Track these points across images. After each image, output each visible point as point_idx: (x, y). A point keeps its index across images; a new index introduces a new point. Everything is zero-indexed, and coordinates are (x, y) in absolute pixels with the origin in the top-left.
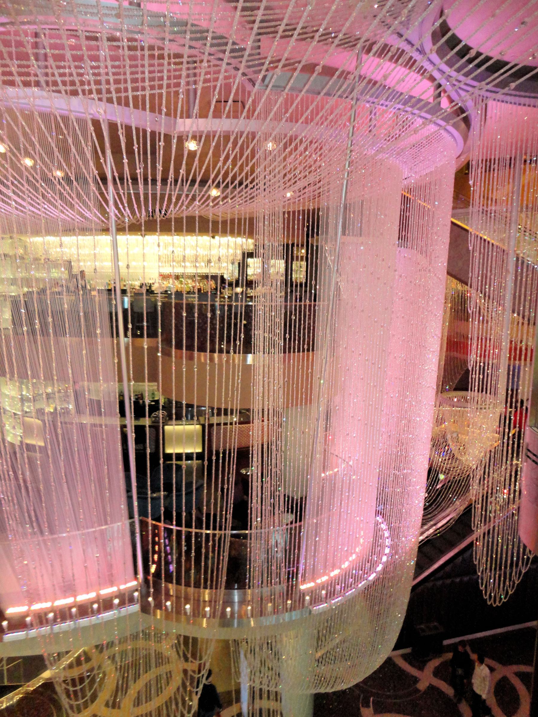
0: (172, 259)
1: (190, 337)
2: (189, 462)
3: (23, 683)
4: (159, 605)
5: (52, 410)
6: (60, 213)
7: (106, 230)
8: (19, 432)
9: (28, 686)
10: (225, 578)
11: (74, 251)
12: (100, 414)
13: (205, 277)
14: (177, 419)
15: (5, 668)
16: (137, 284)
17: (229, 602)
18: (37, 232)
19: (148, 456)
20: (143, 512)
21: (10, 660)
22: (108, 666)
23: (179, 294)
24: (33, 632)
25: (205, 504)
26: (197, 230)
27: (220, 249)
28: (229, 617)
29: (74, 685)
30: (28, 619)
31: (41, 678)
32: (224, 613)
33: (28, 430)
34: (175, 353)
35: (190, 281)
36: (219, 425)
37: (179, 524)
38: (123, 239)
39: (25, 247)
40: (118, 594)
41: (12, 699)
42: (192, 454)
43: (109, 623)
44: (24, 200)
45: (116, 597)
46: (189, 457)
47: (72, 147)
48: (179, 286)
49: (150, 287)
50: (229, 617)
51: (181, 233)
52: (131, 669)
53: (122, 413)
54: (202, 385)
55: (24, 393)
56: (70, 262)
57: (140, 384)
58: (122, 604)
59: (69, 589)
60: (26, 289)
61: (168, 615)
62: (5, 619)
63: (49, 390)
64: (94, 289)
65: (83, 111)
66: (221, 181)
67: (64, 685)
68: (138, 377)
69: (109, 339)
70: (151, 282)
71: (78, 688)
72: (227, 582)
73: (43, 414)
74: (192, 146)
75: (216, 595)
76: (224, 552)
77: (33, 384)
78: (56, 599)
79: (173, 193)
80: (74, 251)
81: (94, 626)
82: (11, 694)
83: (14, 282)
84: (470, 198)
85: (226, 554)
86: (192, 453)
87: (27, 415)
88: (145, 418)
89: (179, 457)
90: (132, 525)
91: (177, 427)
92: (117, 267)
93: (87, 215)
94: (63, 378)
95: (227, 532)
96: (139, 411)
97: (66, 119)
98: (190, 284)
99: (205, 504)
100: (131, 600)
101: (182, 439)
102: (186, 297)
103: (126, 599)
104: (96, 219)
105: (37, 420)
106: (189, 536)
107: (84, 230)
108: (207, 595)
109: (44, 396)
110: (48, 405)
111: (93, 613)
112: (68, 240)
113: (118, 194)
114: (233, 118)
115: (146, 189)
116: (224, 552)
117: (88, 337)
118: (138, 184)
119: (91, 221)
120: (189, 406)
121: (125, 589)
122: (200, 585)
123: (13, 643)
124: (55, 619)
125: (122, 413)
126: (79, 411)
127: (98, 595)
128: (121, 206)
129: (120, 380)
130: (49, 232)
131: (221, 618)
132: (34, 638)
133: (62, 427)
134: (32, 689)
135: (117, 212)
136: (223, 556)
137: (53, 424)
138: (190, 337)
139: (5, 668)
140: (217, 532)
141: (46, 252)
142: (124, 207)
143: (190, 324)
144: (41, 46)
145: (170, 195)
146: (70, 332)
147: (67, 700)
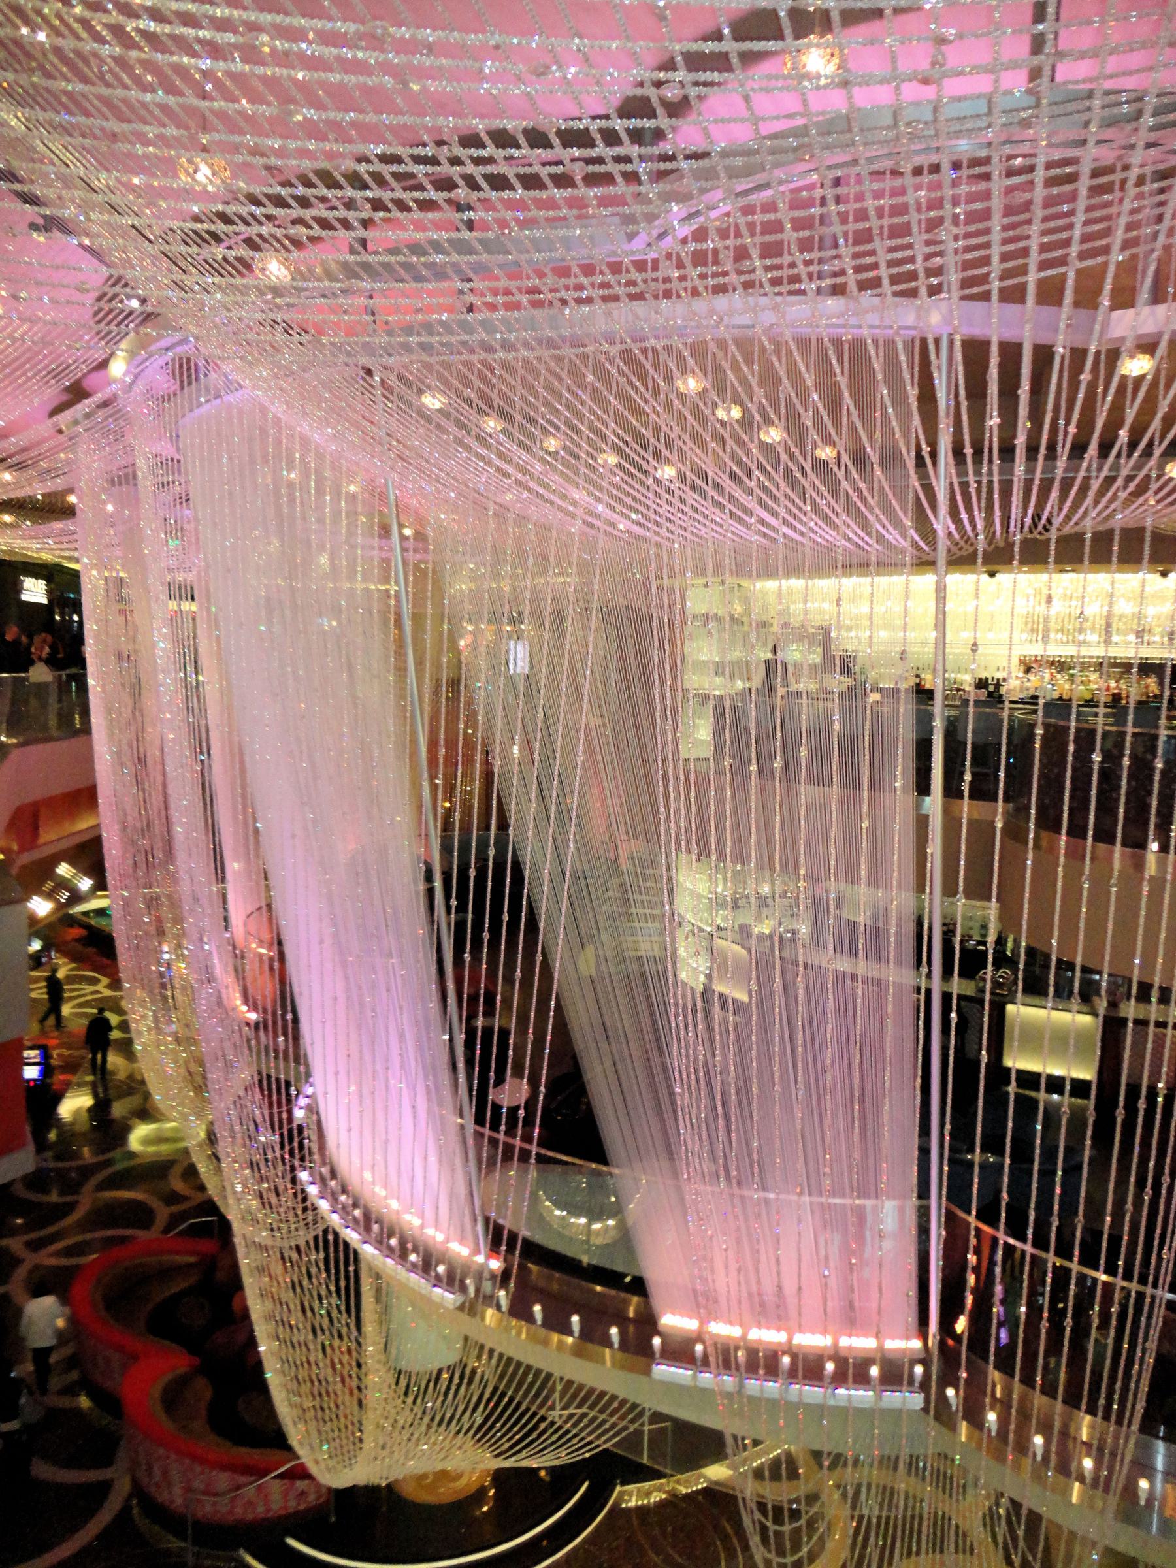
0: (1041, 629)
1: (1107, 808)
2: (1055, 1097)
3: (668, 1471)
4: (974, 1416)
5: (767, 932)
6: (842, 535)
7: (925, 563)
8: (703, 964)
9: (678, 1482)
10: (1140, 1406)
11: (829, 607)
12: (854, 953)
13: (1147, 668)
14: (1058, 994)
15: (646, 1428)
16: (967, 680)
17: (1143, 1467)
18: (768, 572)
19: (983, 1070)
20: (958, 1194)
21: (657, 1417)
22: (835, 1509)
23: (1060, 707)
24: (706, 1379)
25: (1109, 1208)
26: (1115, 559)
28: (1142, 1502)
29: (778, 1520)
30: (699, 1348)
31: (705, 1477)
32: (1130, 1490)
33: (720, 964)
34: (1093, 847)
35: (1094, 676)
36: (1141, 1023)
37: (1041, 1242)
38: (960, 582)
39: (746, 601)
40: (832, 1352)
41: (648, 1494)
42: (1038, 1075)
43: (843, 1413)
45: (830, 1358)
46: (1055, 1084)
47: (846, 394)
48: (1067, 686)
49: (998, 686)
50: (1142, 1502)
51: (1077, 567)
54: (1071, 916)
55: (719, 890)
56: (826, 631)
57: (979, 903)
58: (792, 1374)
59: (769, 1309)
60: (740, 685)
62: (658, 1333)
63: (765, 890)
64: (876, 689)
66: (1157, 435)
67: (758, 1515)
70: (1000, 675)
71: (787, 1528)
72: (1145, 1417)
73: (749, 935)
74: (1137, 366)
75: (1116, 1438)
76: (1146, 1339)
77: (734, 872)
78: (801, 1330)
79: (1094, 474)
80: (829, 607)
81: (820, 1410)
82: (647, 1485)
83: (719, 669)
85: (1152, 1345)
86: (1038, 1075)
87: (722, 934)
88: (974, 983)
89: (1029, 1080)
90: (923, 1214)
91: (1056, 1015)
92: (941, 643)
93: (890, 538)
94: (790, 868)
95: (1159, 1292)
98: (1096, 684)
99: (1109, 1208)
101: (1050, 1041)
102: (1079, 714)
103: (894, 1374)
105: (737, 948)
106: (1062, 1276)
107: (887, 565)
108: (1085, 1427)
109: (753, 900)
110: (759, 919)
112: (825, 585)
113: (964, 486)
115: (1030, 470)
116: (1146, 1339)
117: (788, 780)
118: (1013, 460)
120: (1065, 966)
121: (850, 1348)
122: (1079, 1397)
123: (670, 1387)
124: (705, 1362)
126: (817, 939)
127: (880, 1348)
128: (964, 516)
130: (793, 570)
131: (1122, 1496)
132: (704, 1391)
133: (807, 975)
134: (684, 1491)
135: (952, 527)
136: (1144, 1351)
137: (771, 962)
138: (1107, 808)
139: (646, 1428)
140: (1149, 1290)
141: (786, 611)
143: (1109, 776)
145: (1087, 479)
147: (762, 1548)
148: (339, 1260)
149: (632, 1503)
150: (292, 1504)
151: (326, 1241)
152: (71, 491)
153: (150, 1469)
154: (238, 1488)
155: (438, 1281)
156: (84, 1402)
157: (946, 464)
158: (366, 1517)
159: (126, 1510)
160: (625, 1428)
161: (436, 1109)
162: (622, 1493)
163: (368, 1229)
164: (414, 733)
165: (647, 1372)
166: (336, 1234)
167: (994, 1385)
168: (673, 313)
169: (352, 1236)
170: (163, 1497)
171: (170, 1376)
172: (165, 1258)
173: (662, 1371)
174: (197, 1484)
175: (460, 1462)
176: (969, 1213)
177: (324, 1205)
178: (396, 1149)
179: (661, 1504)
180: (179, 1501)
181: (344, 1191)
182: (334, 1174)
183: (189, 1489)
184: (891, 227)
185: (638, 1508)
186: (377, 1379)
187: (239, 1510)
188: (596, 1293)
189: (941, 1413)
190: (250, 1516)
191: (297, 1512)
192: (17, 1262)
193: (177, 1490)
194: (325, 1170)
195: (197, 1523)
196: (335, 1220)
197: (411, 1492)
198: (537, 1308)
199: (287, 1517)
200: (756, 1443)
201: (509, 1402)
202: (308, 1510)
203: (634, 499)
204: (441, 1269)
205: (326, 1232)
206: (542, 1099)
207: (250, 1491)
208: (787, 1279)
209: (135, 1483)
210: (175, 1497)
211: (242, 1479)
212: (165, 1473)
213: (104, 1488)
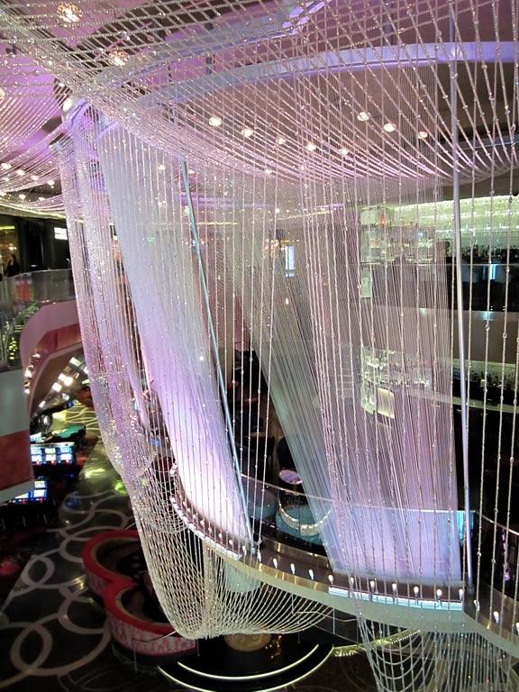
27: (475, 213)
44: (365, 164)
52: (184, 643)
53: (457, 393)
61: (495, 628)
65: (394, 59)
68: (477, 355)
69: (446, 311)
84: (464, 151)
96: (476, 393)
97: (409, 69)
100: (455, 597)
104: (438, 175)
111: (413, 595)
114: (483, 39)
119: (471, 169)
125: (457, 393)
129: (456, 356)
142: (509, 147)
144: (322, 12)
146: (404, 304)
148: (193, 543)
149: (340, 655)
150: (180, 648)
151: (187, 534)
152: (62, 223)
153: (117, 631)
154: (155, 639)
155: (230, 548)
156: (91, 600)
157: (454, 86)
158: (214, 652)
159: (108, 648)
160: (322, 616)
161: (241, 475)
162: (335, 651)
163: (207, 531)
164: (204, 296)
165: (327, 591)
166: (192, 533)
167: (493, 95)
168: (302, 63)
169: (200, 535)
170: (123, 642)
171: (125, 590)
172: (116, 539)
173: (332, 590)
174: (138, 637)
175: (247, 630)
176: (506, 526)
177: (185, 520)
178: (213, 490)
179: (355, 655)
180: (130, 643)
181: (195, 513)
182: (189, 506)
183: (133, 639)
184: (420, 17)
185: (342, 657)
186: (210, 597)
187: (156, 649)
188: (309, 555)
189: (469, 610)
190: (161, 652)
191: (181, 652)
192: (62, 539)
193: (129, 640)
194: (185, 504)
195: (137, 654)
196: (191, 527)
197: (233, 644)
198: (293, 566)
199: (177, 654)
200: (402, 629)
201: (268, 602)
202: (187, 651)
203: (288, 157)
204: (372, 584)
205: (186, 530)
206: (266, 457)
207: (160, 641)
208: (397, 542)
209: (112, 635)
210: (128, 642)
211: (157, 636)
212: (123, 633)
213: (98, 638)
